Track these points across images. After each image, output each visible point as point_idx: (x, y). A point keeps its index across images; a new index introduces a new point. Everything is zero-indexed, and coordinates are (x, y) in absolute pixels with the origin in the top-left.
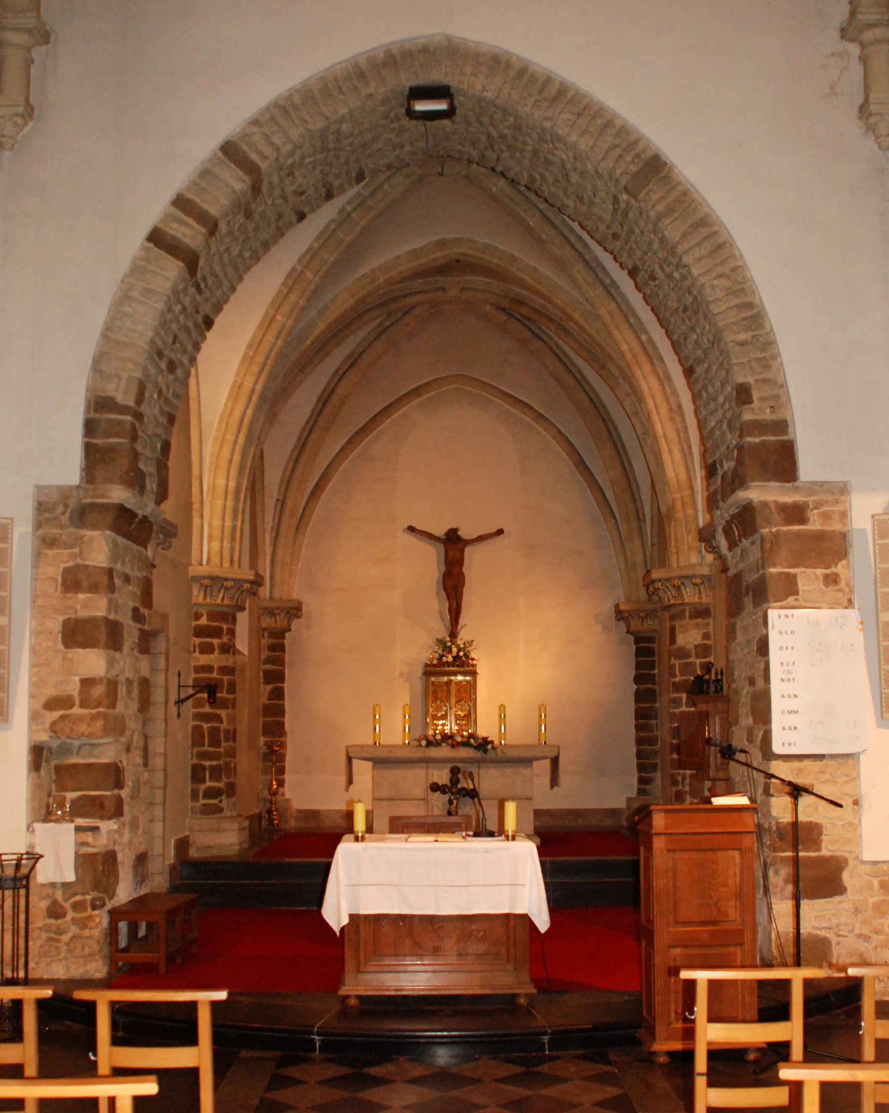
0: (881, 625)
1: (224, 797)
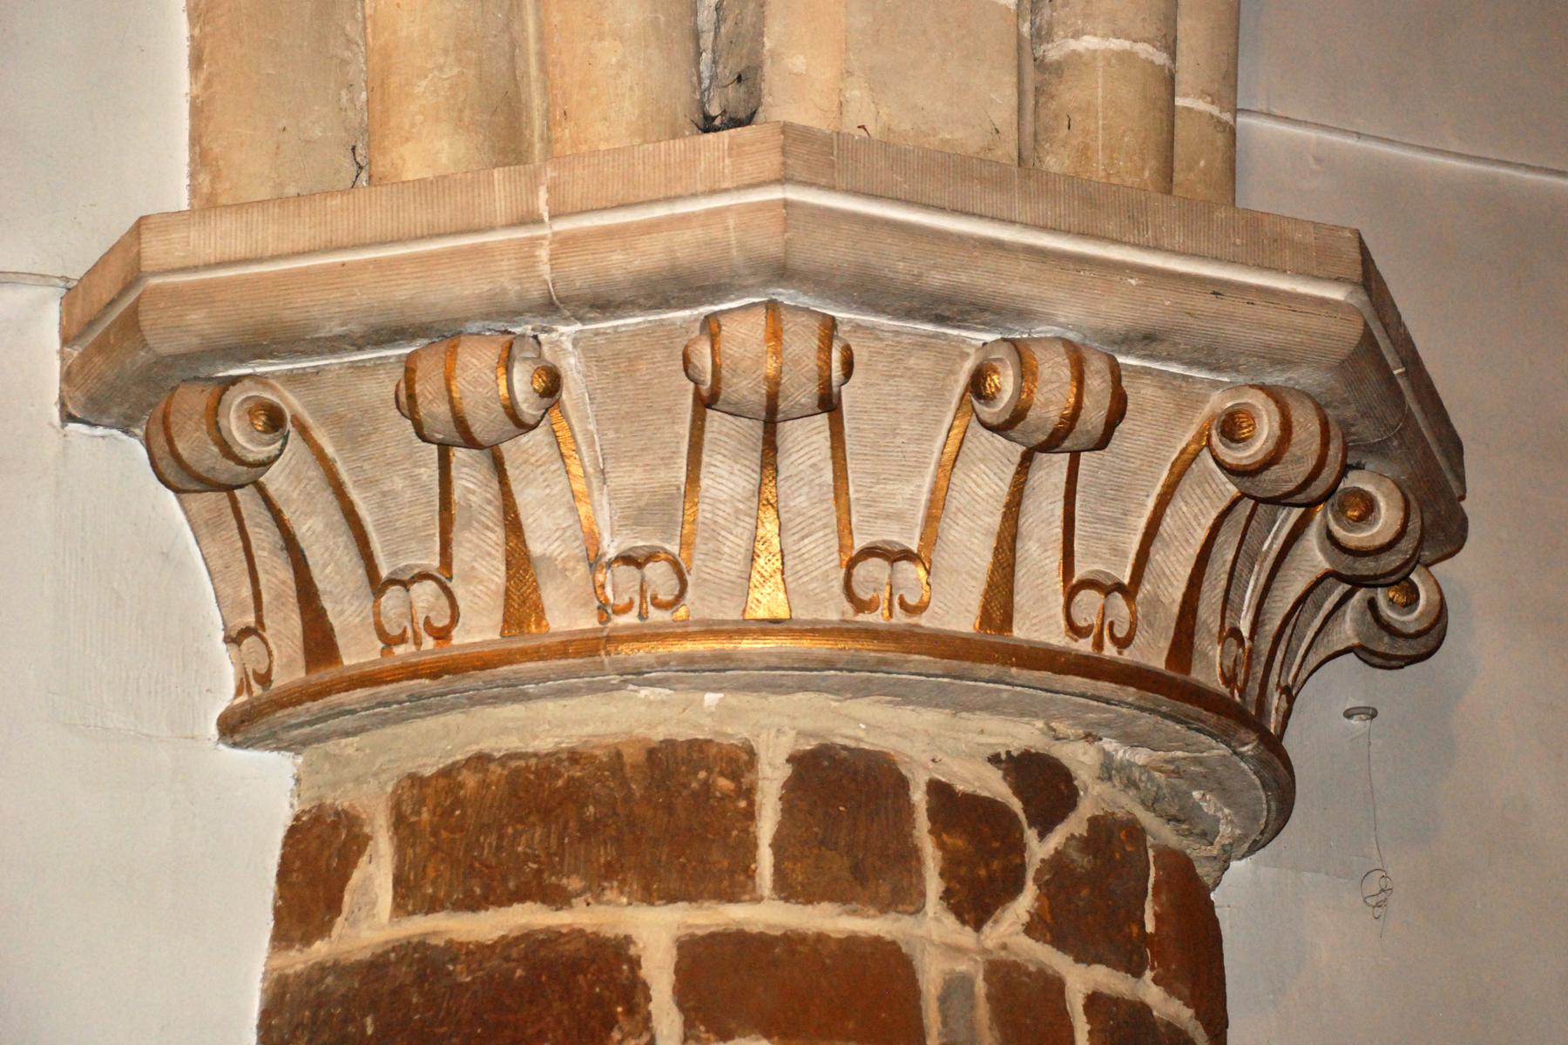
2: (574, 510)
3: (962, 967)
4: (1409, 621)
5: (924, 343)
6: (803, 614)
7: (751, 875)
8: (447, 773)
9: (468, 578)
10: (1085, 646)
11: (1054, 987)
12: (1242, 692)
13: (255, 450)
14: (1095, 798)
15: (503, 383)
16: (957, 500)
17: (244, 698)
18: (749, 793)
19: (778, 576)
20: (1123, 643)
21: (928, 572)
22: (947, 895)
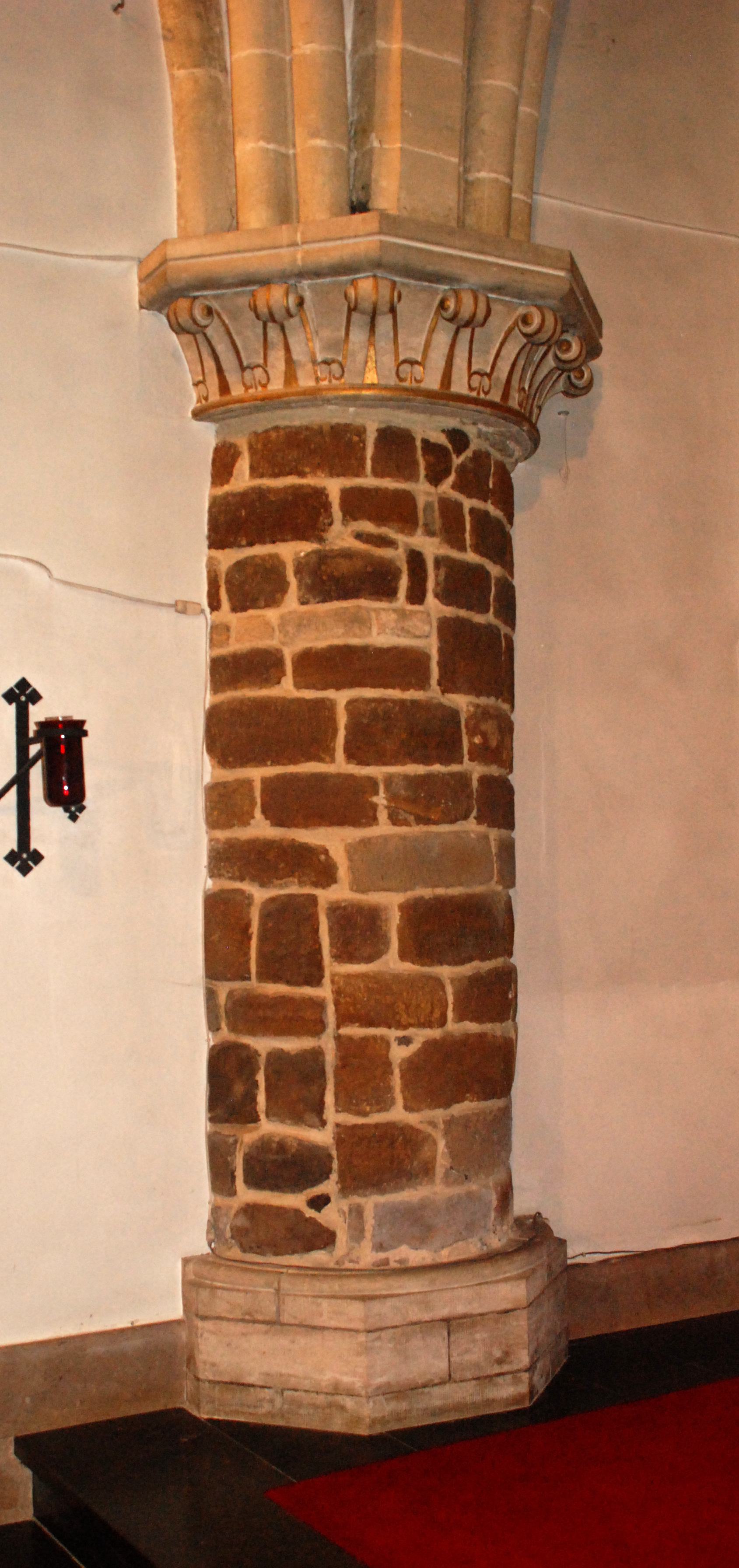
0: (162, 269)
1: (330, 1186)
2: (307, 345)
3: (430, 499)
4: (581, 383)
5: (424, 289)
6: (383, 382)
7: (364, 468)
8: (266, 431)
9: (273, 367)
10: (474, 394)
11: (459, 506)
12: (525, 410)
13: (203, 322)
14: (475, 444)
15: (285, 301)
16: (434, 343)
17: (199, 405)
18: (363, 442)
19: (375, 369)
20: (486, 393)
21: (424, 369)
22: (427, 476)
